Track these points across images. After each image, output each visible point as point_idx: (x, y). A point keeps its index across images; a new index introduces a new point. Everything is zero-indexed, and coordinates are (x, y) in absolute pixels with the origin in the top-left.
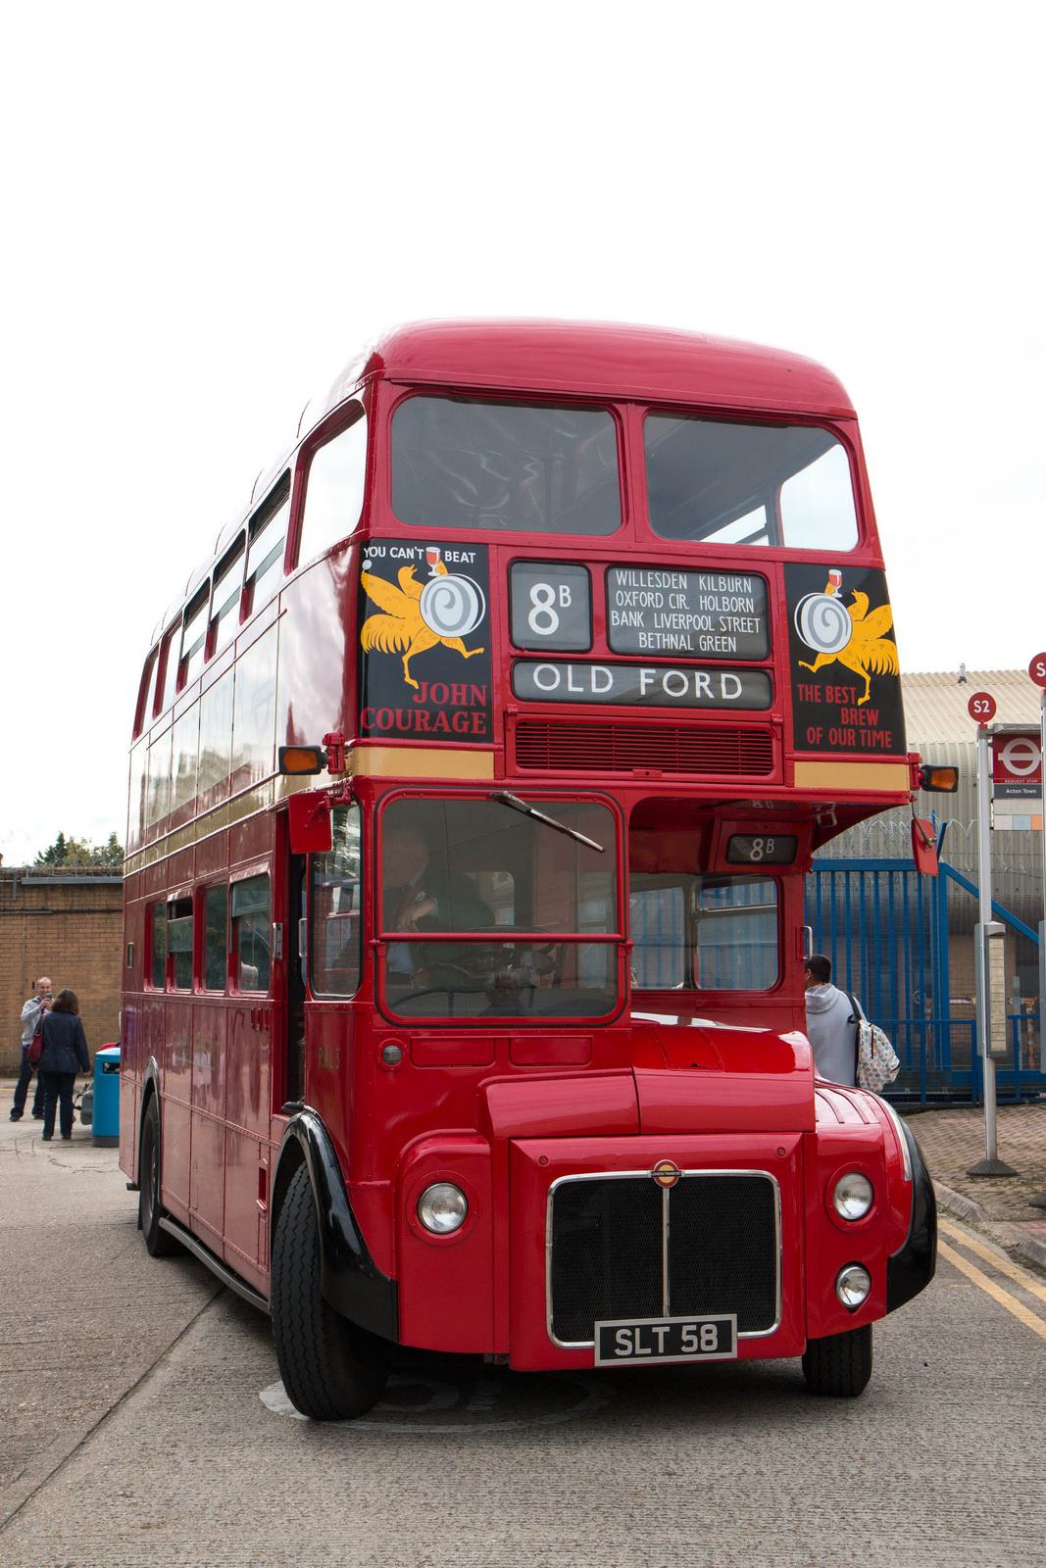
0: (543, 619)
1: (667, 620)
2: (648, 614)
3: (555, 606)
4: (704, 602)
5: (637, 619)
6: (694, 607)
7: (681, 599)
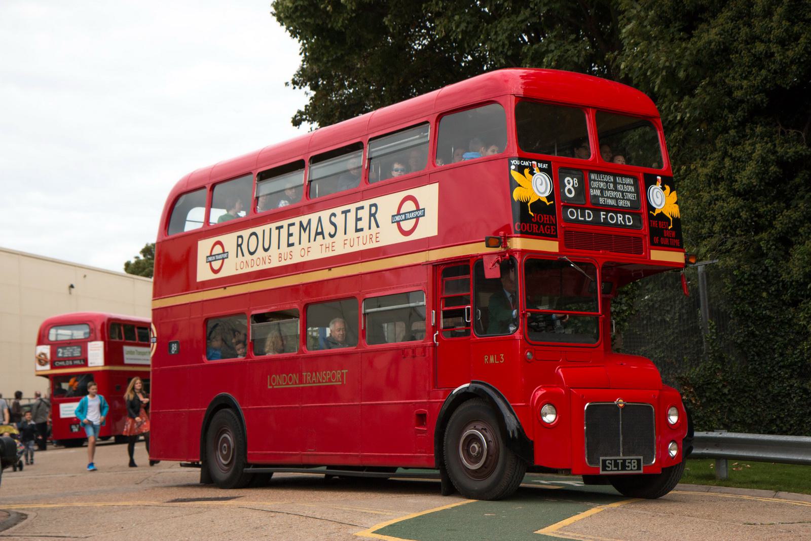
0: (570, 191)
1: (608, 193)
2: (602, 190)
3: (573, 186)
4: (619, 187)
5: (598, 193)
6: (616, 190)
7: (612, 185)
